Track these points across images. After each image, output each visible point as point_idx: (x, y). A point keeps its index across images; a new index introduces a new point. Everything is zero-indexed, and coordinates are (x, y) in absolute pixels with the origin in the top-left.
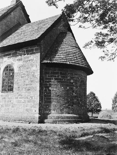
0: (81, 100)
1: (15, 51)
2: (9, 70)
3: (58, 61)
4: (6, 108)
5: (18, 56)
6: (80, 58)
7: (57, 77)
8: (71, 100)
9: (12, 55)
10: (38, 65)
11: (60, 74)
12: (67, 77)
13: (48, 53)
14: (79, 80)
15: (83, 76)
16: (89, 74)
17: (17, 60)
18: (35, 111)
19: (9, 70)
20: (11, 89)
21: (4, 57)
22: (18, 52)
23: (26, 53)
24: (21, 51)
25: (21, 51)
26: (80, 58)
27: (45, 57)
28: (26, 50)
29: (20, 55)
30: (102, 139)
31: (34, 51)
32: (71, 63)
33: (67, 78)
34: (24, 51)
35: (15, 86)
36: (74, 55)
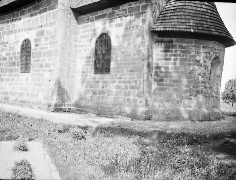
0: (210, 88)
1: (113, 10)
2: (104, 40)
3: (176, 28)
4: (99, 96)
5: (117, 18)
6: (212, 21)
7: (175, 52)
8: (194, 87)
9: (108, 17)
10: (144, 64)
11: (179, 48)
12: (190, 52)
13: (162, 13)
14: (211, 57)
15: (218, 50)
16: (227, 47)
17: (116, 26)
18: (141, 102)
19: (104, 40)
20: (108, 70)
21: (96, 20)
22: (116, 11)
23: (128, 14)
24: (120, 9)
25: (120, 9)
26: (212, 21)
27: (156, 20)
28: (129, 8)
29: (119, 17)
30: (110, 100)
31: (141, 11)
32: (196, 30)
33: (190, 53)
34: (126, 10)
35: (113, 65)
36: (203, 16)
